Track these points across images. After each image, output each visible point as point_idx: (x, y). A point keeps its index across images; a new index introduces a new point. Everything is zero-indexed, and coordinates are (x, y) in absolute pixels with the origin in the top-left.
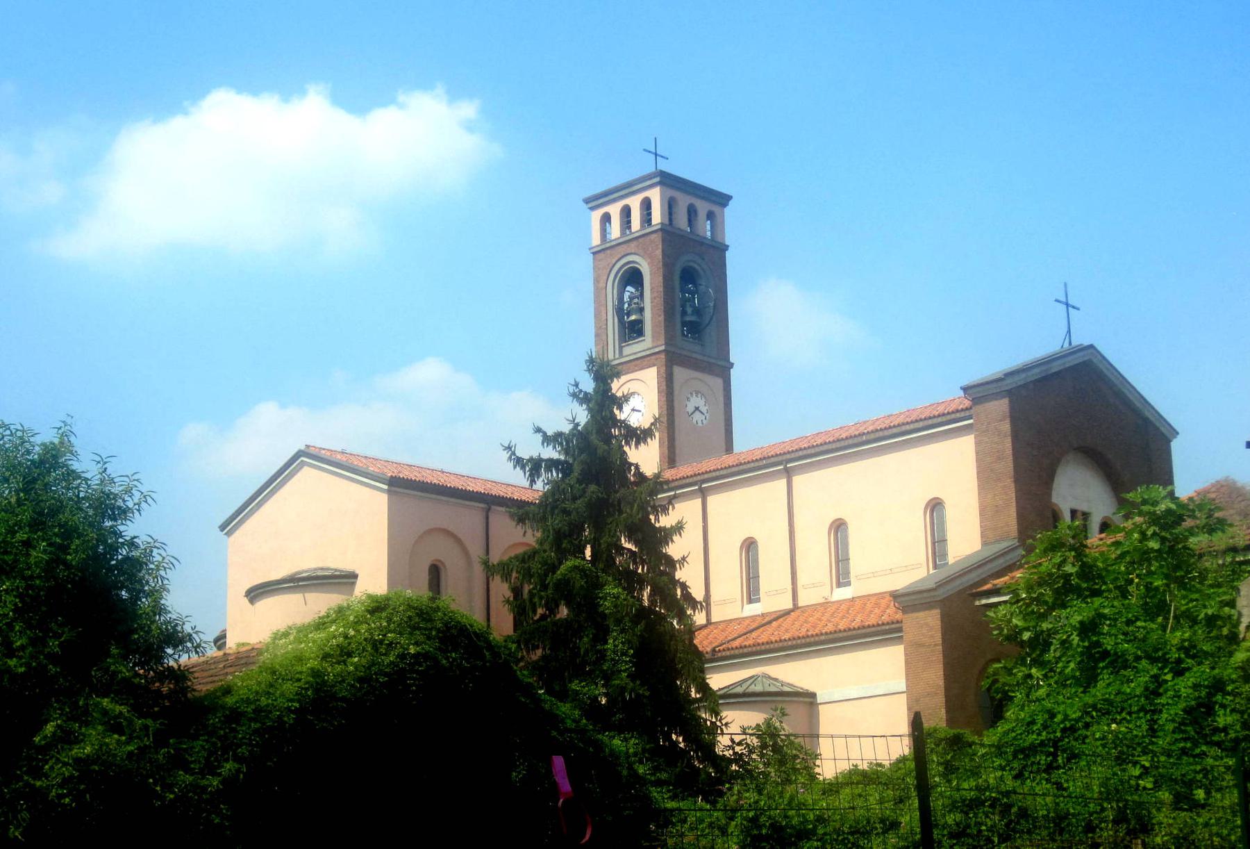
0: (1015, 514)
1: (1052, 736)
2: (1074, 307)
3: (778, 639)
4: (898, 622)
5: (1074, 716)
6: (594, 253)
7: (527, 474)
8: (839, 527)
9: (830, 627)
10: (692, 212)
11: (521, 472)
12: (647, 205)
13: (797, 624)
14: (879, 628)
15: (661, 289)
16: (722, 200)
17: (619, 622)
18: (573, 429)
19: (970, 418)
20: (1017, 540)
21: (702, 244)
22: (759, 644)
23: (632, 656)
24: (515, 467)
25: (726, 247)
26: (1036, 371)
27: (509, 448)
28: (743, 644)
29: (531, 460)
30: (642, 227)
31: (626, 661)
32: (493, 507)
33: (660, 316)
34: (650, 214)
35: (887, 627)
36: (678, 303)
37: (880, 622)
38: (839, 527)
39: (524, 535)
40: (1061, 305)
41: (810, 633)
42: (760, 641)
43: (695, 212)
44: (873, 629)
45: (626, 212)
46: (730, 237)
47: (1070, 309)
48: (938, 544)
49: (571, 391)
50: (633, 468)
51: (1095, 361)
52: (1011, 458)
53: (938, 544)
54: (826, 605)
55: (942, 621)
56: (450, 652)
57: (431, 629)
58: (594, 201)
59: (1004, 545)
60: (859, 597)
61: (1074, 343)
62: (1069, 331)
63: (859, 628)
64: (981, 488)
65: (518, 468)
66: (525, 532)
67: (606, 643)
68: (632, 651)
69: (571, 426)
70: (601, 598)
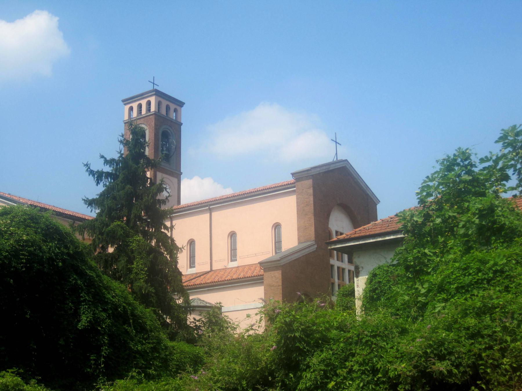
0: (314, 230)
1: (486, 276)
2: (338, 143)
3: (205, 283)
4: (261, 275)
5: (501, 263)
6: (125, 123)
7: (96, 179)
8: (233, 235)
9: (229, 278)
10: (168, 108)
11: (93, 178)
12: (149, 103)
13: (213, 277)
14: (252, 278)
15: (153, 139)
16: (181, 104)
17: (140, 253)
18: (120, 157)
19: (294, 187)
20: (314, 241)
21: (172, 122)
22: (196, 285)
23: (146, 271)
24: (89, 175)
25: (182, 124)
26: (324, 168)
27: (87, 165)
28: (188, 285)
29: (98, 172)
30: (147, 113)
31: (143, 274)
32: (76, 222)
33: (152, 150)
34: (150, 107)
35: (256, 278)
36: (160, 146)
37: (253, 275)
38: (233, 235)
39: (91, 212)
40: (333, 142)
41: (220, 280)
42: (197, 284)
43: (169, 108)
44: (250, 279)
45: (140, 106)
46: (184, 119)
47: (337, 144)
48: (278, 243)
49: (120, 140)
50: (149, 180)
51: (348, 167)
52: (312, 205)
53: (278, 243)
54: (225, 269)
55: (282, 275)
56: (49, 243)
57: (38, 228)
58: (126, 101)
59: (309, 243)
60: (240, 266)
61: (338, 159)
62: (336, 154)
63: (243, 278)
64: (299, 217)
65: (91, 176)
66: (92, 210)
67: (133, 264)
68: (146, 269)
69: (119, 155)
70: (131, 242)
